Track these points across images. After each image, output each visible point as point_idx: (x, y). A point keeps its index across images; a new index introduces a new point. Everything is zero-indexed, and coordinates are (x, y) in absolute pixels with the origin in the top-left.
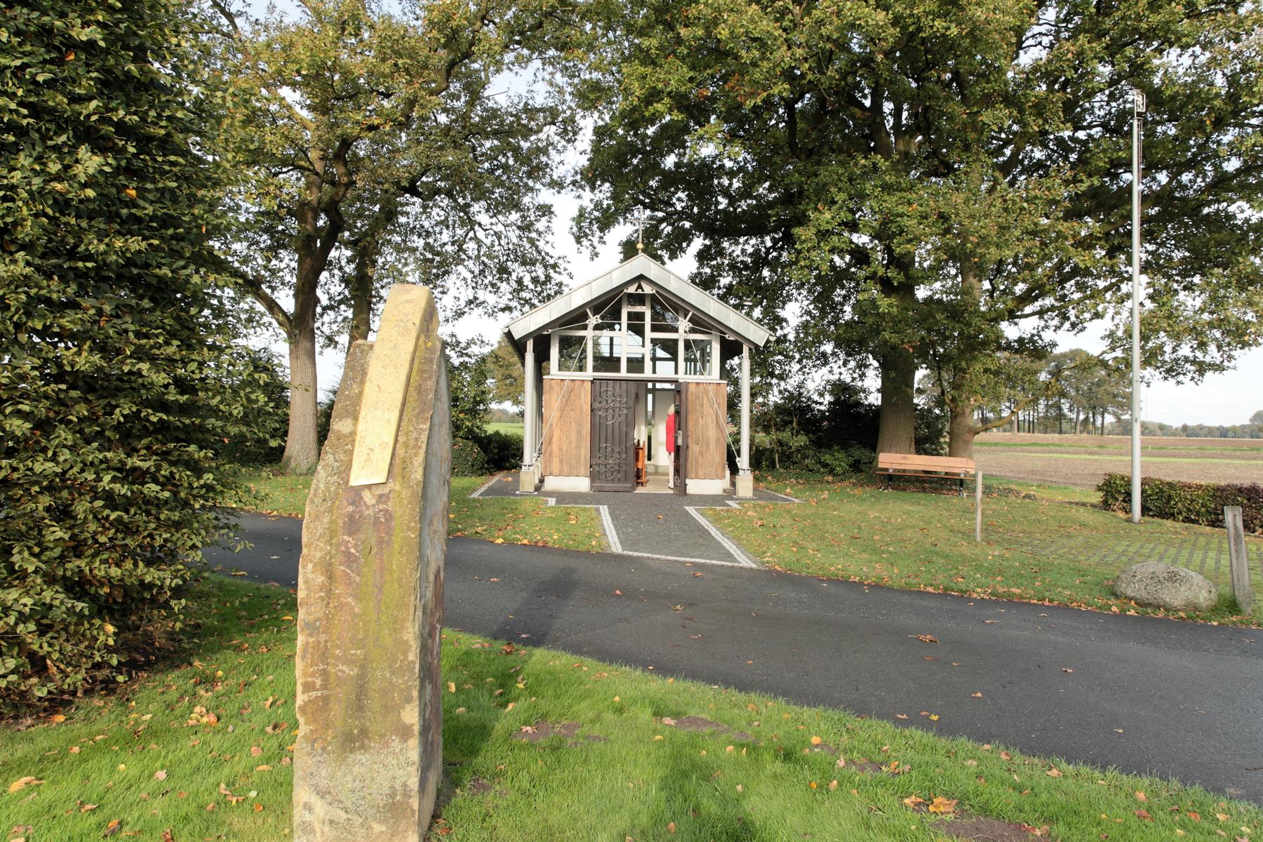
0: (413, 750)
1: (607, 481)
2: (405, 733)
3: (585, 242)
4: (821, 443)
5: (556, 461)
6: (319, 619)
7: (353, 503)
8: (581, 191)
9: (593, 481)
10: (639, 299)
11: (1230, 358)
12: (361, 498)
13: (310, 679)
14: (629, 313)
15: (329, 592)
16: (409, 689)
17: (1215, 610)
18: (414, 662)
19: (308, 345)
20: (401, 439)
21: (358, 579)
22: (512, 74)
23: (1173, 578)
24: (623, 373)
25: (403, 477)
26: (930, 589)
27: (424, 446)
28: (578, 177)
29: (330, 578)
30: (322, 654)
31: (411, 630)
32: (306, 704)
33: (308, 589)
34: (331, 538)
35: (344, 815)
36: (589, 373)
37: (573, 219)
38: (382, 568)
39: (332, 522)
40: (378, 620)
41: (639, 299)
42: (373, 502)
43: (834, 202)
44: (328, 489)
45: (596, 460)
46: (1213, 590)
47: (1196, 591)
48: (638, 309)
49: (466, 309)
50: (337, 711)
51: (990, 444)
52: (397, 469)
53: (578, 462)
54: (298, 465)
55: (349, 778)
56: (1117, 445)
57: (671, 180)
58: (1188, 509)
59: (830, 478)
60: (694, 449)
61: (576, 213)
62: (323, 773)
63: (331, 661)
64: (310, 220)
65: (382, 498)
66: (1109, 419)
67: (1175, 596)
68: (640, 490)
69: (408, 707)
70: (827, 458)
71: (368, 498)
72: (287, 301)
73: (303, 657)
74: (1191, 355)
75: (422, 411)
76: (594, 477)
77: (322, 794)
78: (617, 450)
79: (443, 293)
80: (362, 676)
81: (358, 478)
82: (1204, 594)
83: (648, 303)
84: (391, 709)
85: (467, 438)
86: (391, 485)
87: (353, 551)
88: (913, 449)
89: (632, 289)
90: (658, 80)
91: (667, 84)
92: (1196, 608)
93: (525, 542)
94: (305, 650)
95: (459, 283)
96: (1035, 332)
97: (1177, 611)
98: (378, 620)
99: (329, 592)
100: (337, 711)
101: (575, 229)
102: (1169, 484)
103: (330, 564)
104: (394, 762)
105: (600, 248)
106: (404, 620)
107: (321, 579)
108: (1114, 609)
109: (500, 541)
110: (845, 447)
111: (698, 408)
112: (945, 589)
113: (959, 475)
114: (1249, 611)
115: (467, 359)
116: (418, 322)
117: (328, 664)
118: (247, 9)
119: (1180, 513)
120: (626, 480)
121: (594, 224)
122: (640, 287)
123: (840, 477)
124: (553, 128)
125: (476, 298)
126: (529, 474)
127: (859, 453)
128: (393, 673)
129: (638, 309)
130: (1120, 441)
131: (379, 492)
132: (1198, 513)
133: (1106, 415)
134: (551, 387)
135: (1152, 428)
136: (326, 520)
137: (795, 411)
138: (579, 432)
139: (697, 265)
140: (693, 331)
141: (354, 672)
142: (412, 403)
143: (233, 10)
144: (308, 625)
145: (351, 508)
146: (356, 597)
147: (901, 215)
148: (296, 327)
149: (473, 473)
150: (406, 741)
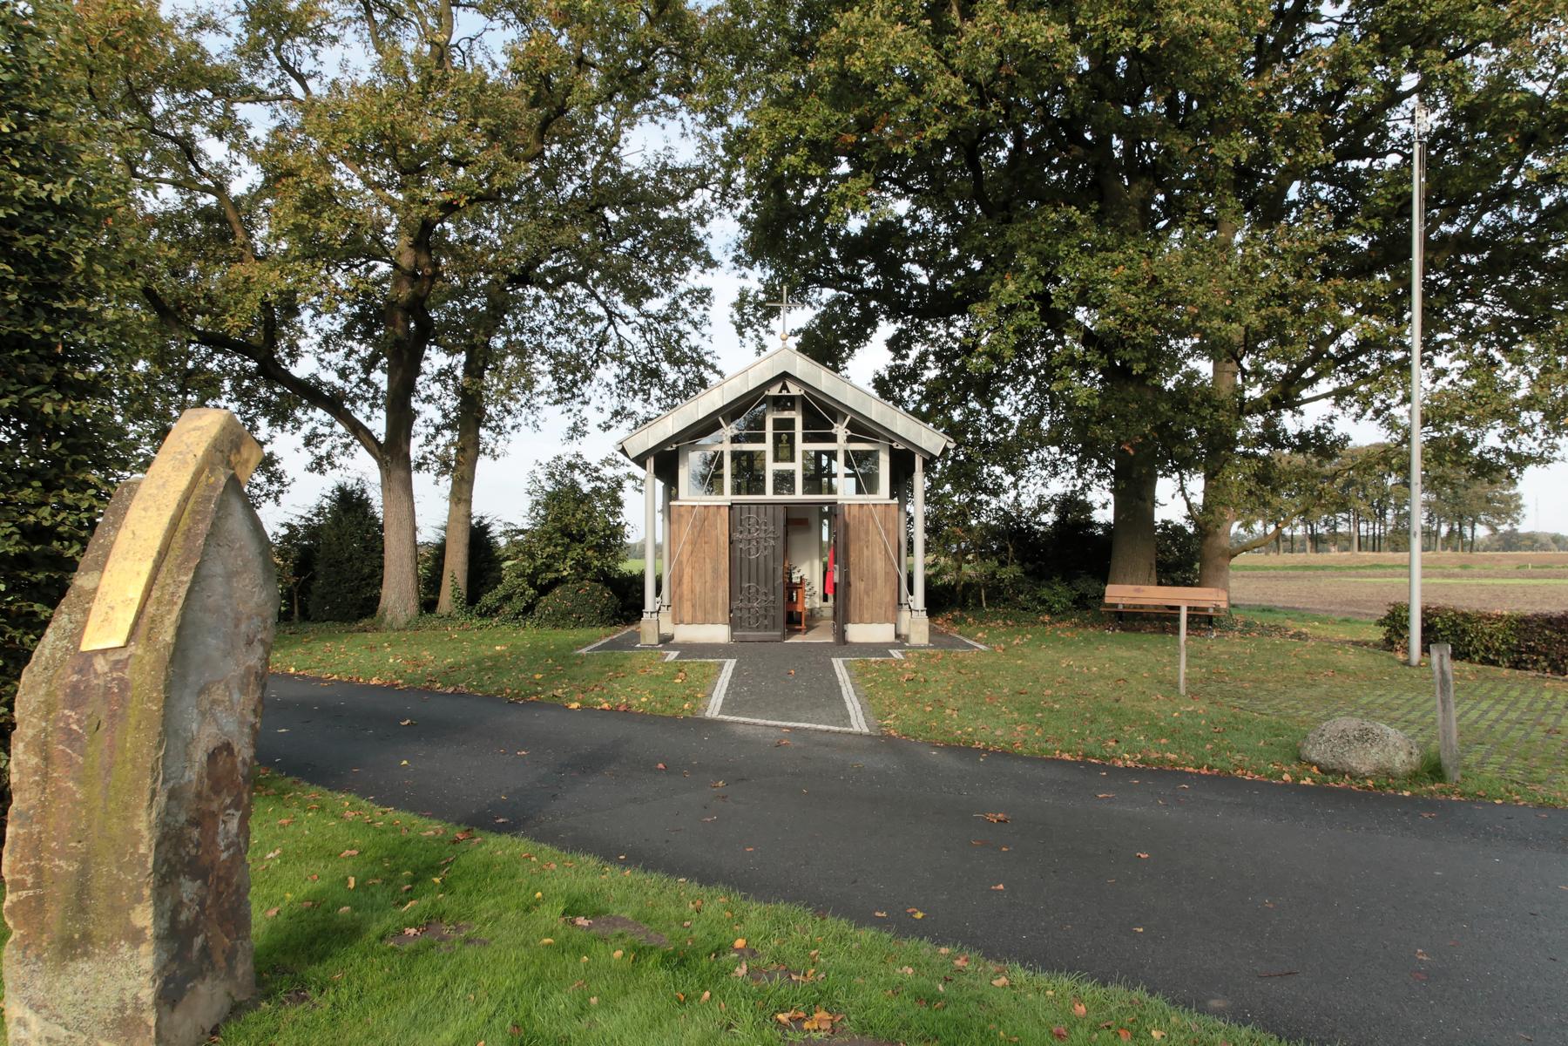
0: (147, 957)
1: (751, 629)
2: (136, 937)
3: (749, 332)
4: (1038, 575)
5: (687, 606)
6: (34, 807)
7: (80, 672)
8: (745, 270)
9: (733, 628)
10: (781, 403)
11: (1554, 447)
12: (92, 665)
13: (18, 877)
14: (775, 421)
15: (46, 776)
16: (139, 886)
17: (1414, 777)
18: (146, 856)
19: (403, 474)
20: (155, 594)
21: (80, 760)
22: (658, 127)
23: (1365, 736)
24: (769, 495)
25: (149, 639)
26: (1066, 756)
27: (180, 602)
28: (742, 252)
29: (46, 759)
30: (36, 847)
31: (144, 817)
32: (14, 905)
33: (20, 772)
34: (48, 713)
35: (64, 1032)
36: (727, 497)
37: (734, 305)
38: (111, 746)
39: (49, 694)
40: (105, 807)
41: (781, 403)
42: (106, 669)
43: (1021, 269)
44: (53, 655)
45: (737, 604)
46: (1416, 751)
47: (1393, 750)
48: (786, 415)
49: (613, 423)
50: (53, 913)
51: (1317, 568)
52: (143, 629)
53: (714, 605)
54: (395, 618)
55: (69, 989)
56: (1487, 565)
57: (854, 248)
58: (1487, 649)
59: (1047, 618)
60: (858, 586)
61: (736, 298)
62: (39, 983)
63: (46, 855)
64: (400, 323)
65: (118, 665)
66: (1482, 532)
67: (1364, 760)
68: (797, 639)
69: (139, 908)
70: (1045, 593)
71: (100, 665)
72: (378, 425)
73: (12, 852)
74: (1502, 446)
75: (187, 560)
76: (734, 624)
77: (37, 1008)
78: (763, 590)
79: (585, 403)
80: (83, 872)
81: (92, 641)
82: (1403, 755)
83: (798, 406)
84: (119, 910)
85: (598, 581)
86: (132, 649)
87: (75, 727)
88: (1154, 578)
89: (775, 391)
90: (791, 126)
91: (802, 131)
92: (1390, 774)
93: (606, 706)
94: (14, 843)
95: (601, 390)
96: (1320, 423)
97: (1365, 778)
98: (105, 807)
99: (46, 776)
100: (53, 913)
101: (737, 317)
102: (1465, 615)
103: (45, 743)
104: (123, 971)
105: (767, 339)
106: (137, 807)
107: (34, 761)
108: (1286, 777)
109: (575, 705)
110: (1068, 578)
111: (863, 535)
112: (1085, 756)
113: (1205, 609)
114: (1457, 777)
115: (599, 484)
116: (200, 453)
117: (41, 859)
118: (318, 68)
119: (1476, 652)
120: (774, 628)
121: (755, 313)
122: (785, 387)
123: (1058, 616)
124: (707, 194)
125: (623, 408)
126: (656, 620)
127: (1084, 585)
128: (120, 868)
129: (786, 415)
130: (1493, 558)
131: (116, 657)
132: (1498, 652)
133: (1477, 526)
134: (680, 516)
135: (1544, 540)
136: (41, 692)
137: (1013, 535)
138: (715, 571)
139: (891, 355)
140: (850, 439)
141: (74, 867)
142: (176, 551)
143: (304, 70)
144: (19, 814)
145: (75, 678)
146: (78, 781)
147: (1105, 281)
148: (387, 453)
149: (603, 623)
150: (137, 947)
